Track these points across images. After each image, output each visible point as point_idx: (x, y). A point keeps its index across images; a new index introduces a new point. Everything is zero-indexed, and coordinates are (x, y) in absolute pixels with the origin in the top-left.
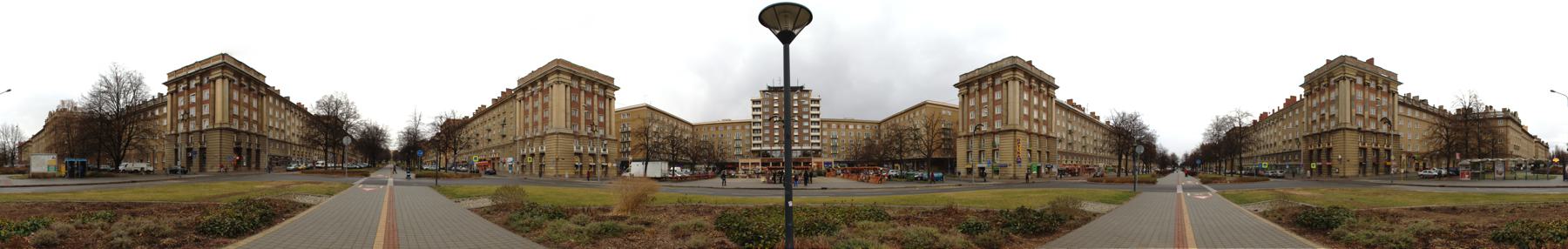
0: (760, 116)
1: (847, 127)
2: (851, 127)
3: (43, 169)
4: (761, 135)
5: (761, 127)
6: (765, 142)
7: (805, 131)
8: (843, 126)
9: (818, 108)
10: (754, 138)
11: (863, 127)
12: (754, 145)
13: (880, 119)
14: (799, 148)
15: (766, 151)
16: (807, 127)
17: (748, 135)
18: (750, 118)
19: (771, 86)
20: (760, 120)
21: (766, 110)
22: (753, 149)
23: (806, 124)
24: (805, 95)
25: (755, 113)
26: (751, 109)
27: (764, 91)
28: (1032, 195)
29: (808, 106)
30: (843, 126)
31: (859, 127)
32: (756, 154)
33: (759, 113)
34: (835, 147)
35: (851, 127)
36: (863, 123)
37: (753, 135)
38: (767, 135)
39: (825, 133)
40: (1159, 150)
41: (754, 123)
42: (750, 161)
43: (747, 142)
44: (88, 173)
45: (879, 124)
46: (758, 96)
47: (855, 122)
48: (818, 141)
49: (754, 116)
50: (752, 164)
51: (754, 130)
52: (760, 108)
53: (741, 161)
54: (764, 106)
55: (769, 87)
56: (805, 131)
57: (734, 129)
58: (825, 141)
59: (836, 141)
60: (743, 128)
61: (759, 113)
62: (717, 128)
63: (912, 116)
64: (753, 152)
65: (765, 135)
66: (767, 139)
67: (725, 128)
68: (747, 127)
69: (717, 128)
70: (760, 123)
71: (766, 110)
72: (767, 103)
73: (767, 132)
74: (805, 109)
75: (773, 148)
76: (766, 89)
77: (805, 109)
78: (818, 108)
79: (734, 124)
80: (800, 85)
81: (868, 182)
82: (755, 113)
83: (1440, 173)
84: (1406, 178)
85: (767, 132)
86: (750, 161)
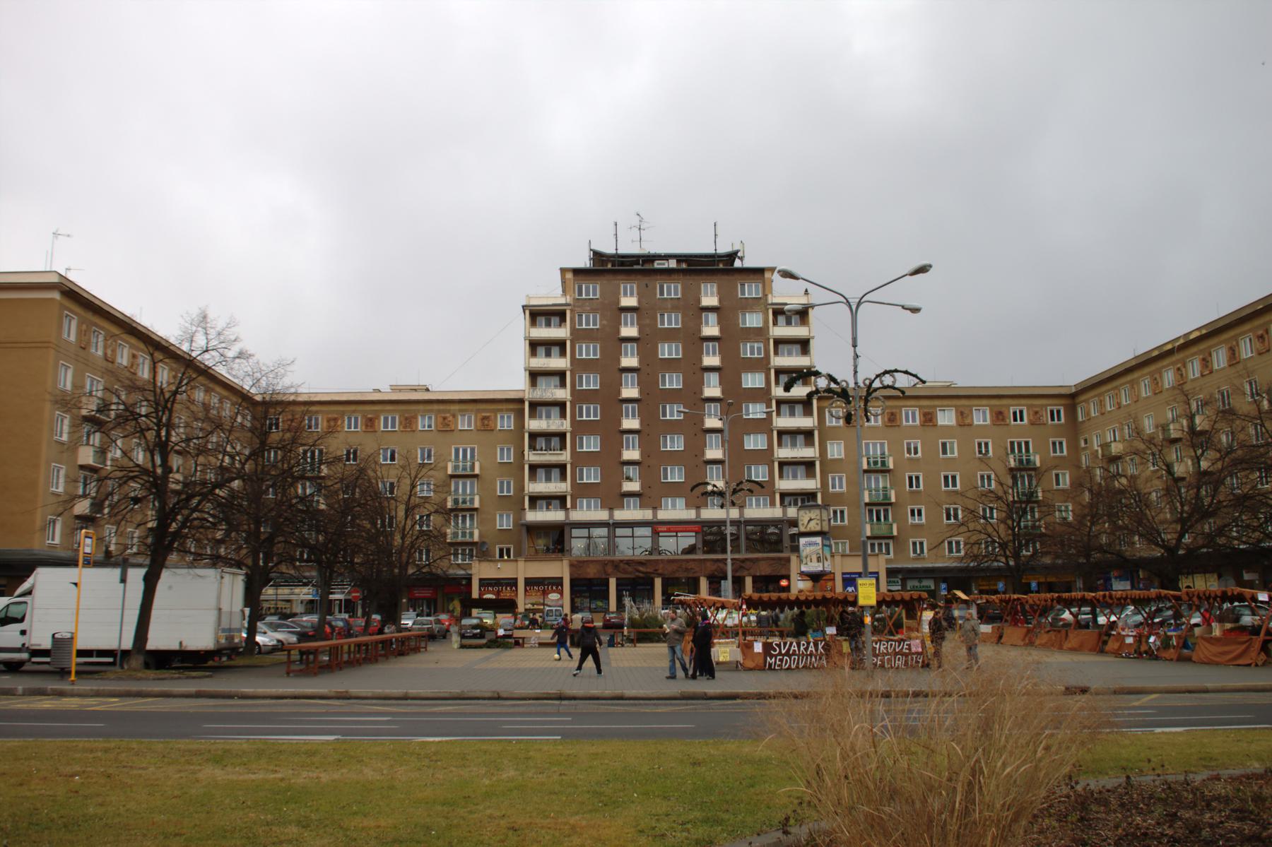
0: (561, 374)
1: (929, 419)
2: (946, 418)
3: (202, 638)
4: (565, 456)
5: (565, 425)
6: (582, 491)
7: (754, 442)
8: (911, 417)
9: (804, 345)
10: (534, 468)
11: (999, 416)
12: (535, 500)
13: (1071, 376)
14: (647, 515)
15: (763, 524)
16: (763, 426)
17: (509, 457)
18: (513, 381)
19: (609, 249)
20: (563, 394)
21: (588, 351)
22: (534, 516)
23: (755, 411)
24: (750, 290)
25: (541, 362)
26: (522, 348)
27: (577, 272)
28: (78, 755)
29: (760, 333)
30: (911, 417)
31: (981, 417)
32: (541, 543)
33: (557, 362)
34: (880, 507)
35: (946, 418)
36: (998, 399)
37: (532, 457)
38: (590, 459)
39: (836, 450)
40: (169, 464)
41: (534, 405)
42: (523, 570)
43: (504, 488)
44: (328, 648)
45: (1072, 398)
46: (551, 293)
47: (963, 399)
48: (810, 484)
49: (535, 376)
50: (530, 582)
51: (534, 436)
52: (561, 344)
53: (482, 570)
54: (578, 335)
55: (598, 256)
56: (754, 442)
57: (446, 428)
58: (839, 485)
59: (882, 482)
60: (486, 426)
61: (557, 362)
62: (370, 423)
63: (1194, 369)
64: (535, 530)
65: (581, 459)
66: (591, 476)
67: (409, 422)
68: (505, 422)
69: (370, 423)
70: (561, 405)
71: (588, 351)
72: (591, 322)
73: (591, 444)
74: (750, 350)
75: (620, 515)
76: (584, 261)
77: (750, 350)
78: (804, 345)
79: (446, 407)
80: (723, 249)
81: (1182, 659)
82: (541, 362)
83: (534, 614)
84: (1139, 654)
85: (591, 444)
86: (523, 570)
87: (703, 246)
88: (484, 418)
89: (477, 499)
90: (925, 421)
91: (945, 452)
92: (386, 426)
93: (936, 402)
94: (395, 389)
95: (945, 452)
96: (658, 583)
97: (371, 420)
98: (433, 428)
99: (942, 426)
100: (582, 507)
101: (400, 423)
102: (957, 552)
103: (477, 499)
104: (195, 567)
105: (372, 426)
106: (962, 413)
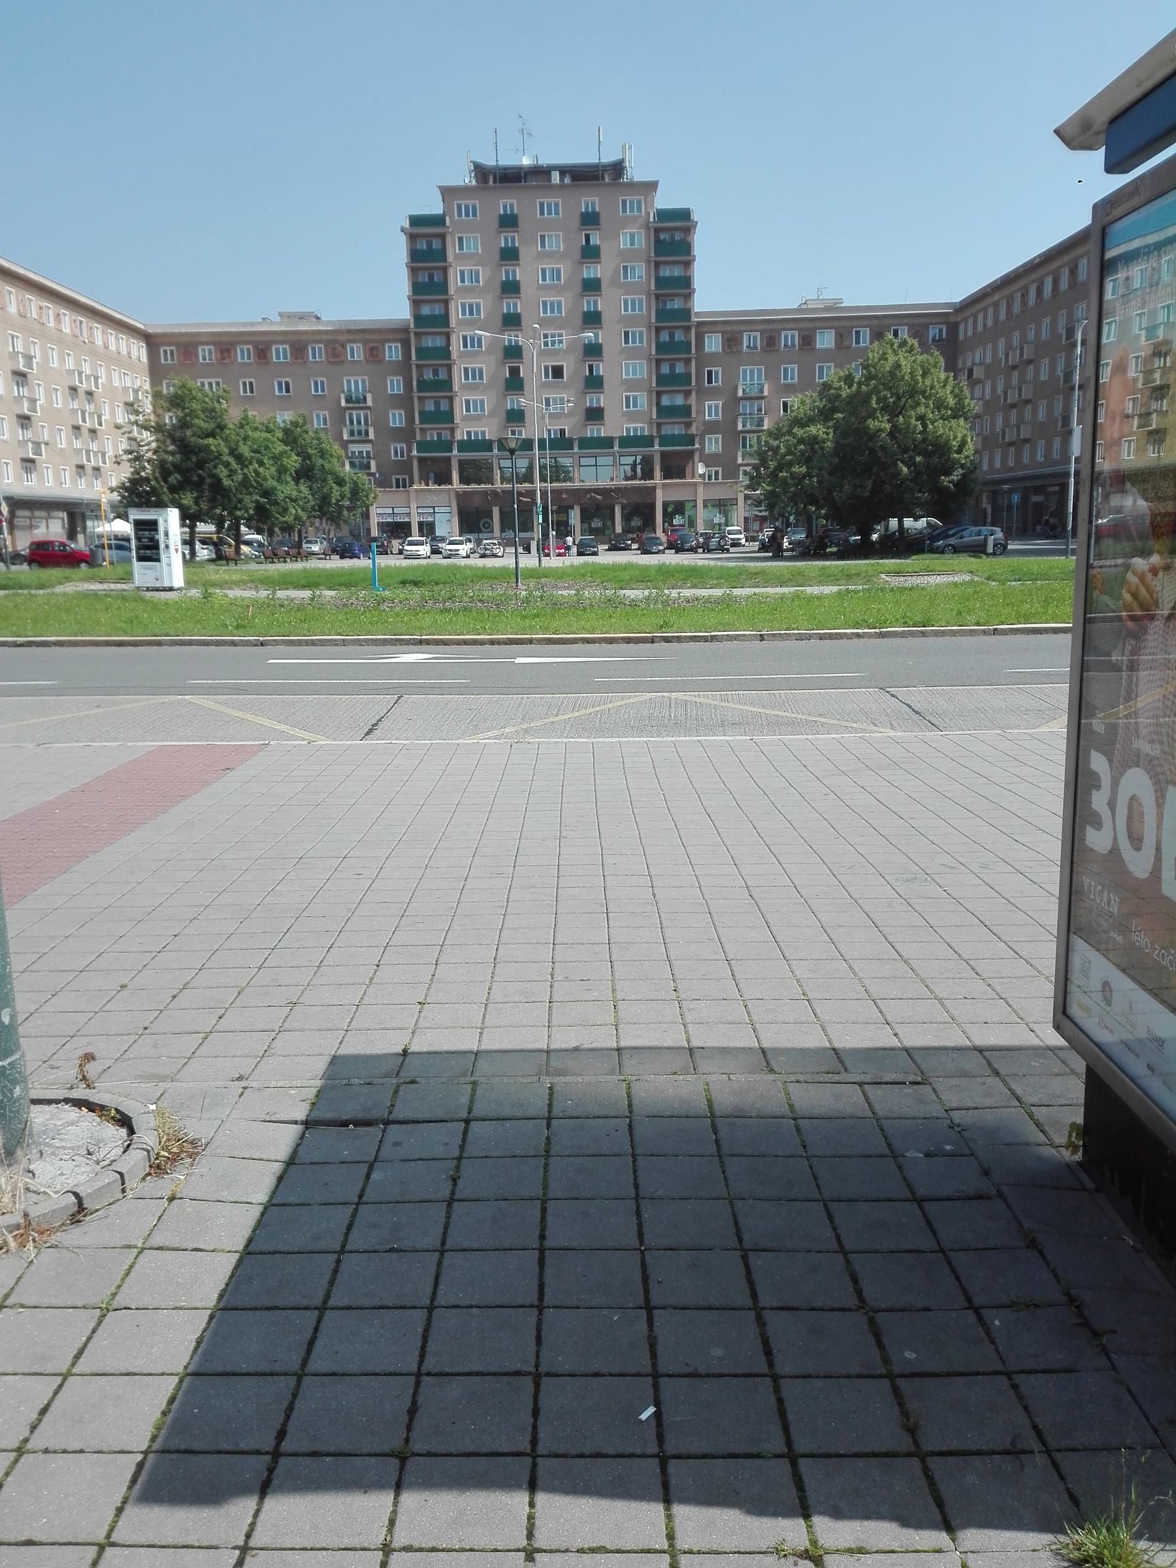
60: (374, 354)
80: (608, 158)
87: (585, 156)
88: (372, 349)
89: (371, 431)
90: (803, 345)
91: (710, 382)
92: (314, 357)
93: (817, 324)
94: (286, 316)
95: (710, 382)
96: (496, 511)
97: (262, 351)
98: (214, 361)
99: (820, 350)
100: (555, 431)
101: (292, 354)
102: (643, 478)
103: (371, 431)
104: (597, 491)
105: (265, 357)
106: (841, 336)
